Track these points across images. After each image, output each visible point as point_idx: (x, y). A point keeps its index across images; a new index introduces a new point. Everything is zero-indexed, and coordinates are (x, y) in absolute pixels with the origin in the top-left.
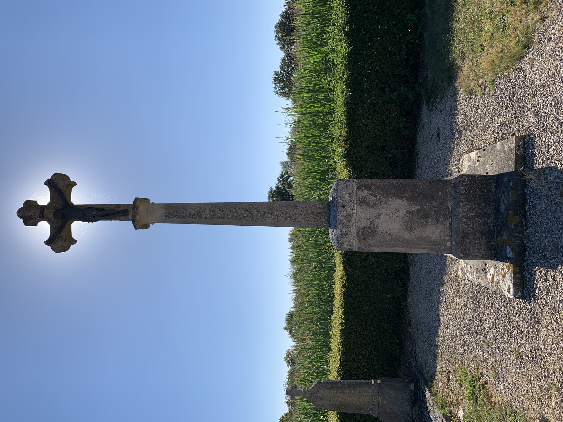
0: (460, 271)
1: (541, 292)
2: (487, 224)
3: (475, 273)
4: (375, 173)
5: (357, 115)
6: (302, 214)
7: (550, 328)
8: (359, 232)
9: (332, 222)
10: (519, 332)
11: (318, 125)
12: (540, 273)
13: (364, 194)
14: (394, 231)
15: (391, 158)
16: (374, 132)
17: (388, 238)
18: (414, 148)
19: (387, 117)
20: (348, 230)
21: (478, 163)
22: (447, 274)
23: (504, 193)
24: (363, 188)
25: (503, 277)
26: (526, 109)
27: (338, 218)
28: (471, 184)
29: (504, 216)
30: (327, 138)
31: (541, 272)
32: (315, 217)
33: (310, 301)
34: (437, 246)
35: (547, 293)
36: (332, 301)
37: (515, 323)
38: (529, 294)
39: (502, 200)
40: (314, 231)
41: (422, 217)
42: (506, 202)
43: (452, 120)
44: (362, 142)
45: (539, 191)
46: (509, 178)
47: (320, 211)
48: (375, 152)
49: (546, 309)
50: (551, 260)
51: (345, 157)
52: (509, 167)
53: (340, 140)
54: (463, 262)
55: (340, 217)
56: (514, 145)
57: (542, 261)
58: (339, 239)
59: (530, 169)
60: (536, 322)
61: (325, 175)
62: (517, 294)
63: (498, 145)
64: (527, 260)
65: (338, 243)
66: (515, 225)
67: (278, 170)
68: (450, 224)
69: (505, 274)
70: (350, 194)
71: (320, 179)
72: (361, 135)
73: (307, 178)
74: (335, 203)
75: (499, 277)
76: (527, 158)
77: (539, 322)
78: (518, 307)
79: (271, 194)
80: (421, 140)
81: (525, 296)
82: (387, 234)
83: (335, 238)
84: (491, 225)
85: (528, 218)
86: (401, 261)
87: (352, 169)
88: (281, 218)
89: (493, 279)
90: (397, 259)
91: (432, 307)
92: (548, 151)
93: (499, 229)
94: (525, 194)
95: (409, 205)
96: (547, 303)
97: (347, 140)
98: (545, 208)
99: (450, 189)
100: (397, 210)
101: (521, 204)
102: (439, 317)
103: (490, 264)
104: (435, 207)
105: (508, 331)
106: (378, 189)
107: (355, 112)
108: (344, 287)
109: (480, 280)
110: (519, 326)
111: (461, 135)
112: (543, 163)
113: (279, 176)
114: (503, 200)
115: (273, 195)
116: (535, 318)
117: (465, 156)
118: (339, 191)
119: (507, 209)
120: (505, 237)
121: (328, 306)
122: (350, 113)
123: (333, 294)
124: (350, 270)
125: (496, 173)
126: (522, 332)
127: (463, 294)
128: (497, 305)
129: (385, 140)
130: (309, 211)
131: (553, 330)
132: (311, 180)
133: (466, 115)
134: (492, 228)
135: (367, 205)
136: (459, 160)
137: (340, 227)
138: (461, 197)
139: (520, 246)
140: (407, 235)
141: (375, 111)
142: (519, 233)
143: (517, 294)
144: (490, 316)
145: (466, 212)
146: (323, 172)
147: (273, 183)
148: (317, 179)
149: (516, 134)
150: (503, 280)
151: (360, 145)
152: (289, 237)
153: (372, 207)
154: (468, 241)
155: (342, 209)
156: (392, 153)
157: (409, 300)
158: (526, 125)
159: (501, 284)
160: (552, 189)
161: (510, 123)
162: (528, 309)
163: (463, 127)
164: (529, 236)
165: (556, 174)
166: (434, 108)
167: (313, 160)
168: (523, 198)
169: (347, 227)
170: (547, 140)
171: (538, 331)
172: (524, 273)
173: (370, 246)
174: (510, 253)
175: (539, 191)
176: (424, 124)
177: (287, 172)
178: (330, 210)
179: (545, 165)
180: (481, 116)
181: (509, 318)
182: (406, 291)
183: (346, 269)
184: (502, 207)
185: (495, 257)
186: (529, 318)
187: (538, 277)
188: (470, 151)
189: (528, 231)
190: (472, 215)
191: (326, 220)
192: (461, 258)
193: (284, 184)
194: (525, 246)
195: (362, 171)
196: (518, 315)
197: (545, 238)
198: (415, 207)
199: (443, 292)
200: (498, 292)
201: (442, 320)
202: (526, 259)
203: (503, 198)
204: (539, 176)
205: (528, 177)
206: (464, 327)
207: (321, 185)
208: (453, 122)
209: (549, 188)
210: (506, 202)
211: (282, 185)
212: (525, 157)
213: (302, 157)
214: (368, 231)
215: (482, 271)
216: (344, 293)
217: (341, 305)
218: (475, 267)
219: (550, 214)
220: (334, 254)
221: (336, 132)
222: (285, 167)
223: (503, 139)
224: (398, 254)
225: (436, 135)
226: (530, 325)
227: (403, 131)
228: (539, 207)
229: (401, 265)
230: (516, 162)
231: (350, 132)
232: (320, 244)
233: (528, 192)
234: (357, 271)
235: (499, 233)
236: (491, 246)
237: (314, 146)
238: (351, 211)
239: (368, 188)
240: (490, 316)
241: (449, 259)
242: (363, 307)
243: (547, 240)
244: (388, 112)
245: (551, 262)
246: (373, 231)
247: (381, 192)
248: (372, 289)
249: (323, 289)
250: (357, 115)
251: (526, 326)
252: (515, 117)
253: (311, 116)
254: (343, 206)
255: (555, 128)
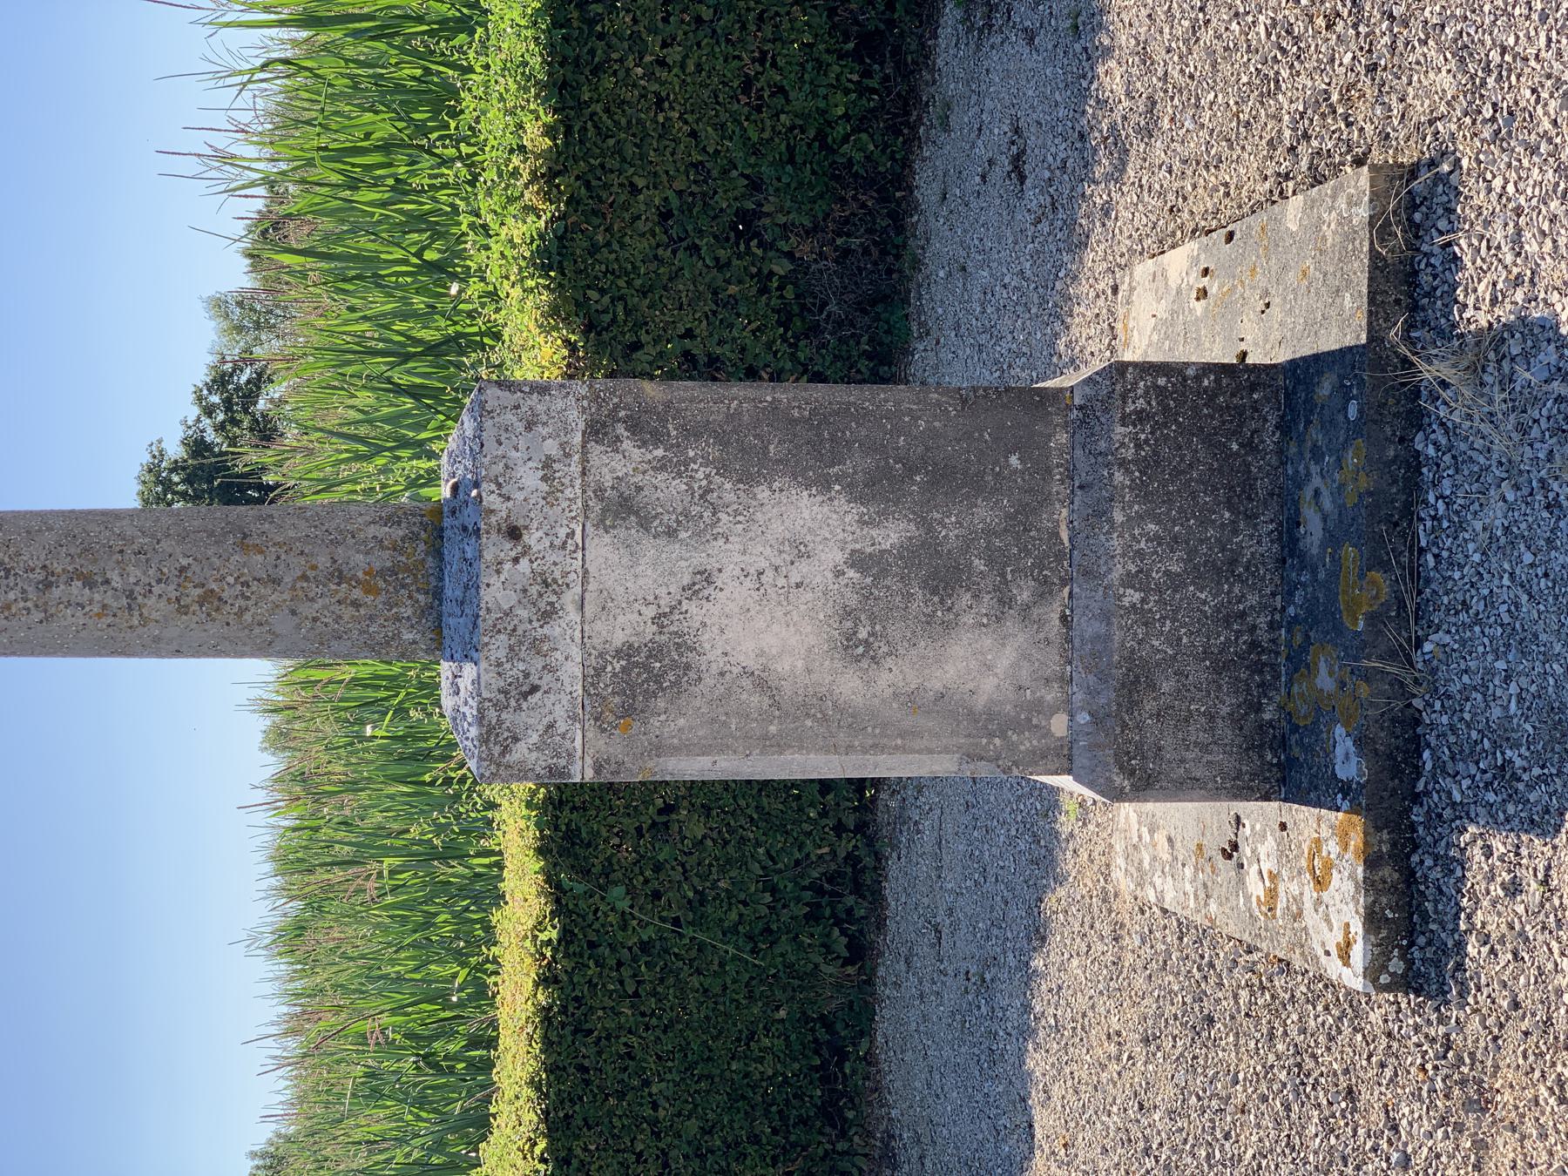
0: (1120, 861)
1: (1492, 951)
2: (1242, 615)
3: (1188, 871)
4: (703, 359)
5: (601, 36)
6: (276, 581)
7: (1530, 1128)
8: (598, 672)
9: (454, 622)
10: (1395, 1157)
11: (399, 88)
12: (1485, 853)
13: (623, 462)
14: (783, 666)
15: (784, 281)
16: (693, 134)
17: (756, 701)
18: (900, 229)
19: (762, 61)
20: (539, 663)
21: (1199, 307)
22: (1060, 880)
23: (1317, 454)
24: (621, 429)
25: (1320, 883)
26: (1417, 31)
27: (487, 596)
28: (1166, 409)
29: (1322, 576)
30: (446, 162)
31: (1488, 852)
32: (357, 593)
33: (371, 1075)
34: (1003, 736)
35: (1515, 954)
36: (487, 1065)
37: (1377, 1118)
38: (1438, 964)
39: (1308, 493)
40: (394, 682)
41: (924, 585)
42: (1327, 503)
43: (1080, 83)
44: (635, 190)
45: (1479, 443)
46: (1341, 377)
47: (382, 559)
48: (702, 243)
49: (1512, 1034)
50: (1530, 787)
51: (545, 269)
52: (1343, 326)
53: (515, 173)
54: (1133, 817)
55: (496, 593)
56: (1362, 213)
57: (1491, 797)
58: (492, 715)
59: (1441, 333)
60: (1468, 1104)
61: (443, 367)
62: (1384, 968)
63: (1293, 210)
64: (1427, 793)
65: (484, 741)
66: (1372, 618)
67: (193, 350)
68: (1063, 618)
69: (1329, 866)
70: (548, 463)
71: (414, 392)
72: (630, 150)
73: (345, 385)
74: (468, 516)
75: (1302, 874)
76: (1425, 278)
77: (1482, 1103)
78: (1389, 1035)
79: (161, 482)
80: (936, 187)
81: (1419, 974)
82: (746, 682)
83: (470, 712)
84: (1262, 621)
85: (1428, 581)
86: (839, 828)
87: (586, 333)
88: (155, 607)
89: (1272, 894)
90: (824, 814)
91: (994, 1057)
92: (1517, 240)
93: (1299, 639)
94: (1414, 463)
95: (862, 523)
96: (1516, 1005)
97: (551, 175)
98: (1507, 529)
99: (1063, 438)
100: (801, 550)
101: (1396, 516)
102: (1026, 1110)
103: (1260, 815)
104: (989, 532)
105: (1344, 1159)
106: (698, 436)
107: (591, 23)
108: (546, 980)
109: (1213, 907)
110: (1395, 1128)
111: (1124, 163)
112: (1494, 301)
113: (202, 376)
114: (1317, 493)
115: (168, 485)
116: (1463, 1082)
117: (1143, 269)
118: (490, 445)
119: (1332, 539)
120: (1325, 680)
121: (470, 1095)
122: (566, 24)
123: (493, 1024)
124: (579, 888)
125: (1282, 356)
126: (1407, 1158)
127: (1139, 982)
128: (1293, 1031)
129: (755, 185)
130: (323, 561)
131: (1544, 1136)
132: (365, 398)
133: (1145, 58)
134: (1263, 636)
135: (644, 525)
136: (1115, 290)
137: (498, 647)
138: (1119, 477)
139: (1393, 720)
140: (849, 685)
141: (699, 20)
142: (1392, 655)
143: (1384, 968)
144: (1263, 1088)
145: (1140, 554)
146: (432, 349)
147: (168, 417)
148: (398, 390)
149: (1376, 157)
150: (1319, 902)
151: (626, 207)
152: (266, 722)
153: (671, 533)
154: (1150, 706)
155: (508, 549)
156: (790, 255)
157: (884, 1025)
158: (1420, 109)
159: (1311, 919)
160: (1535, 432)
161: (1346, 99)
162: (1433, 1040)
163: (1134, 118)
164: (1434, 671)
165: (1549, 355)
166: (998, 20)
167: (378, 281)
168: (1410, 474)
169: (536, 646)
170: (1510, 189)
171: (1480, 1145)
172: (1415, 858)
173: (659, 749)
174: (1348, 764)
175: (1479, 443)
176: (948, 106)
177: (247, 359)
178: (439, 555)
179: (1505, 313)
180: (1214, 64)
181: (1350, 1091)
182: (869, 982)
183: (558, 886)
184: (1313, 530)
185: (1283, 781)
186: (1439, 1085)
187: (1475, 875)
188: (1165, 244)
189: (1428, 647)
190: (1167, 573)
191: (423, 612)
192: (1118, 795)
193: (236, 423)
194: (1418, 722)
195: (637, 346)
196: (1388, 1072)
197: (1507, 679)
198: (892, 535)
199: (1044, 976)
200: (1297, 964)
201: (1044, 1121)
202: (1420, 786)
203: (1316, 481)
204: (1476, 369)
205: (1429, 372)
206: (1147, 1152)
207: (422, 427)
208: (1084, 94)
209: (1523, 429)
210: (1327, 503)
211: (220, 428)
212: (1416, 273)
213: (309, 262)
214: (646, 667)
215: (1220, 860)
216: (545, 1014)
217: (531, 1083)
218: (1189, 838)
219: (1528, 558)
220: (492, 806)
221: (495, 126)
222: (240, 329)
223: (1318, 180)
224: (826, 786)
225: (1005, 162)
226: (1443, 1121)
227: (846, 139)
228: (1478, 526)
229: (845, 846)
230: (1372, 300)
231: (568, 132)
232: (427, 755)
233: (1431, 451)
234: (618, 891)
235: (1299, 662)
236: (1261, 727)
237: (384, 204)
238: (552, 557)
239: (644, 428)
240: (1263, 1088)
241: (1069, 805)
242: (647, 1083)
243: (1513, 689)
244: (768, 30)
245: (1533, 797)
246: (674, 665)
247: (714, 452)
248: (695, 981)
249: (441, 998)
250: (601, 36)
251: (1427, 1126)
252: (1372, 68)
253: (356, 34)
254: (514, 533)
255: (1546, 125)
